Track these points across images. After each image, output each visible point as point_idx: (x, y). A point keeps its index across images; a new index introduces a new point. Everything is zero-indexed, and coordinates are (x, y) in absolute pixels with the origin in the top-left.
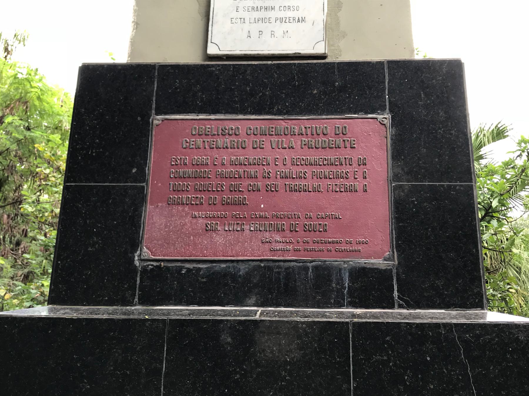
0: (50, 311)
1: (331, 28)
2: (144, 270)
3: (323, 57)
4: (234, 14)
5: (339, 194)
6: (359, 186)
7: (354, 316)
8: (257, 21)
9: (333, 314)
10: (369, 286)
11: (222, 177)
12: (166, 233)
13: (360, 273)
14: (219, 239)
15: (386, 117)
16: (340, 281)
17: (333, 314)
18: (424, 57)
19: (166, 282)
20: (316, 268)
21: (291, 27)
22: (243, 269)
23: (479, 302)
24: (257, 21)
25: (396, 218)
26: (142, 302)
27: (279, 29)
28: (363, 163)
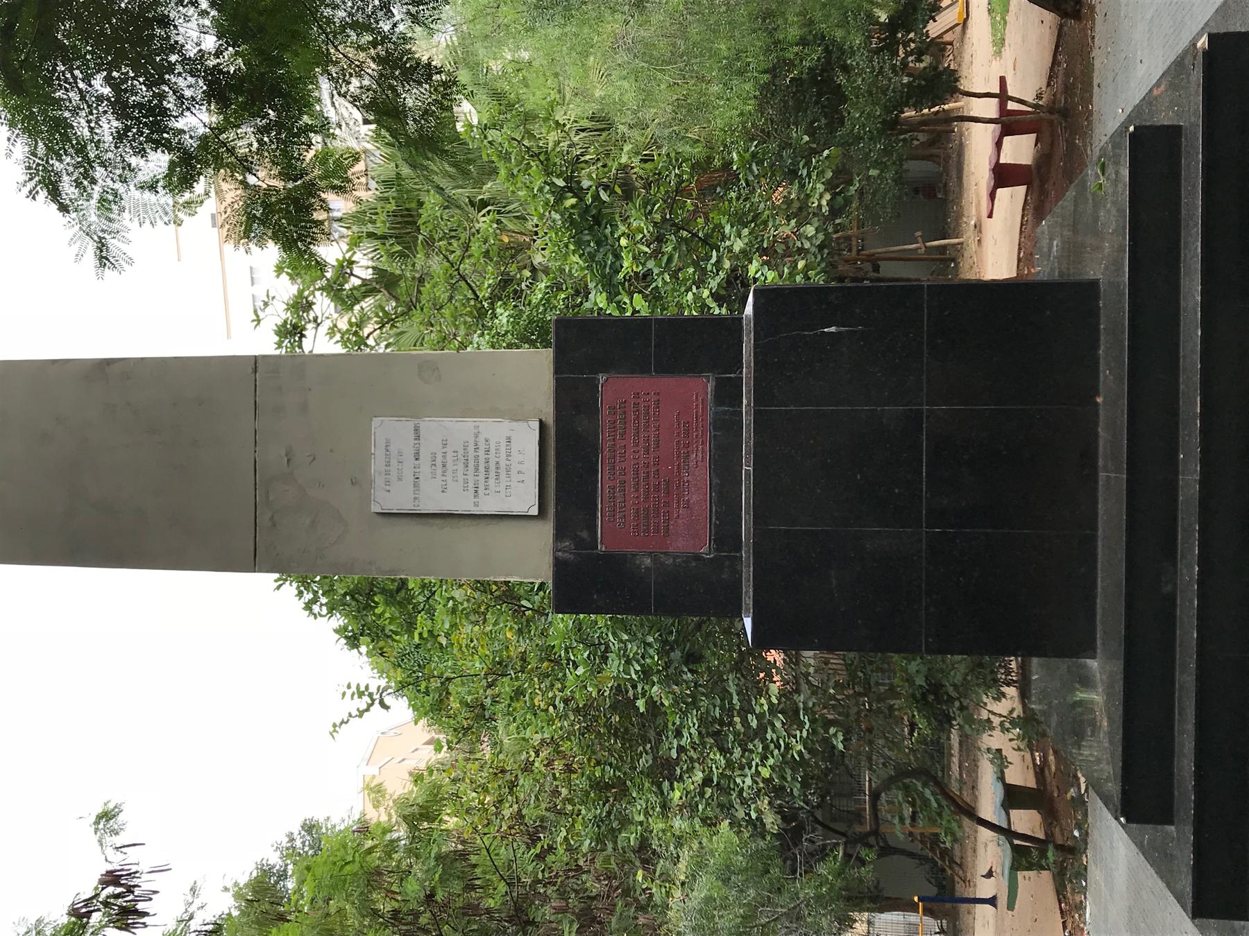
0: (748, 610)
1: (517, 416)
2: (717, 550)
3: (543, 426)
4: (503, 494)
5: (667, 432)
6: (656, 398)
7: (748, 405)
8: (509, 476)
9: (747, 419)
10: (728, 393)
11: (647, 498)
12: (688, 535)
13: (719, 398)
14: (694, 498)
15: (602, 378)
16: (725, 413)
17: (747, 419)
18: (33, 195)
19: (726, 537)
20: (715, 429)
21: (515, 447)
22: (716, 481)
23: (733, 326)
24: (509, 476)
25: (643, 373)
26: (740, 550)
27: (516, 457)
28: (637, 395)
